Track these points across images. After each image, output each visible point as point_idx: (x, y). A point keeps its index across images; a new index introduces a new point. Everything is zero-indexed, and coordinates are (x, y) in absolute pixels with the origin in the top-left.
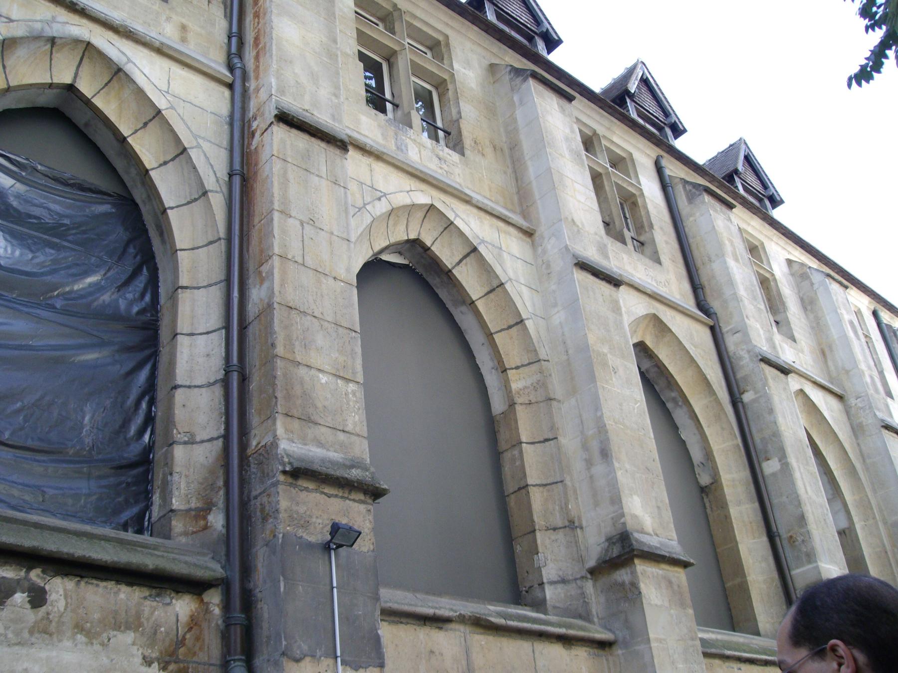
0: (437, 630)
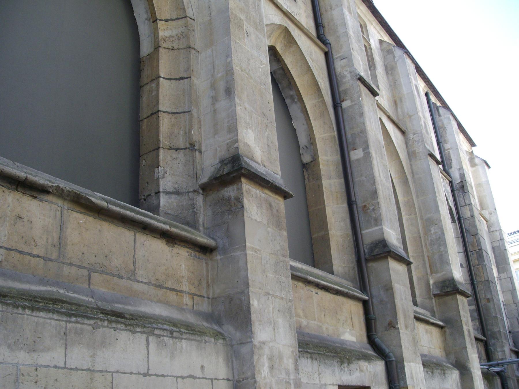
0: (30, 198)
